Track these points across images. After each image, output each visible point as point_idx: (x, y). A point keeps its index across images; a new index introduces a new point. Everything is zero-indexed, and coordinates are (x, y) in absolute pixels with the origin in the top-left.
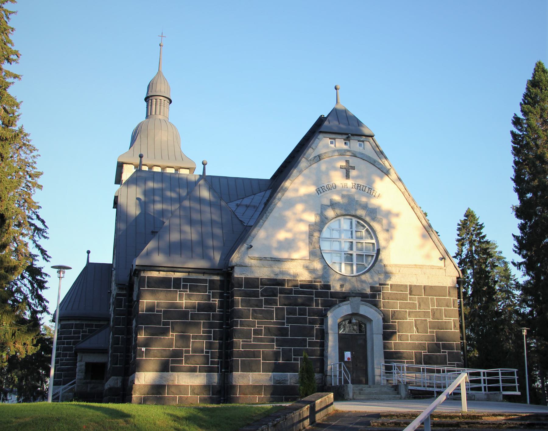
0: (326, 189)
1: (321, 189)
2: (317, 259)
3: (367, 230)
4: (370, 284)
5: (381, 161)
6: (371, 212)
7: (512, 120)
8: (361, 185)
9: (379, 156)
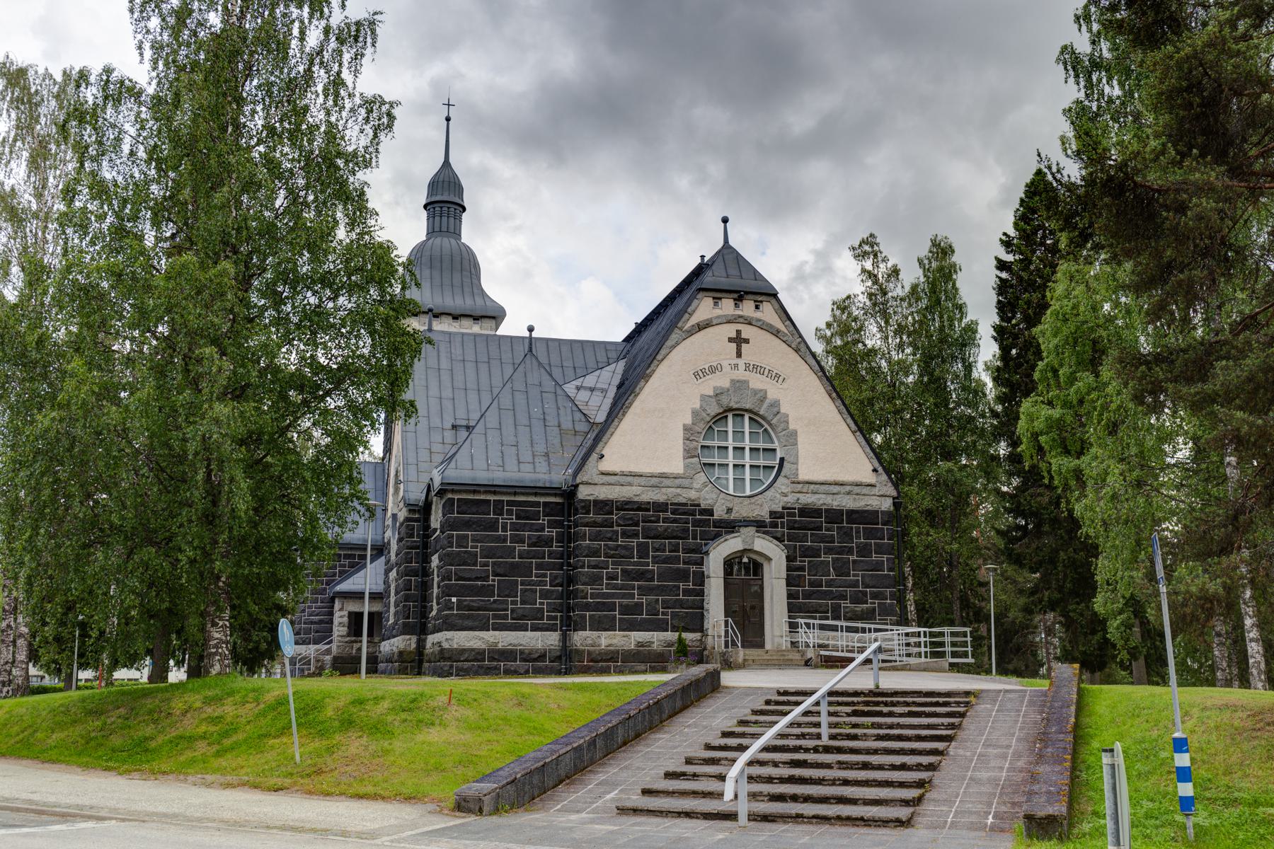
7: (1001, 240)
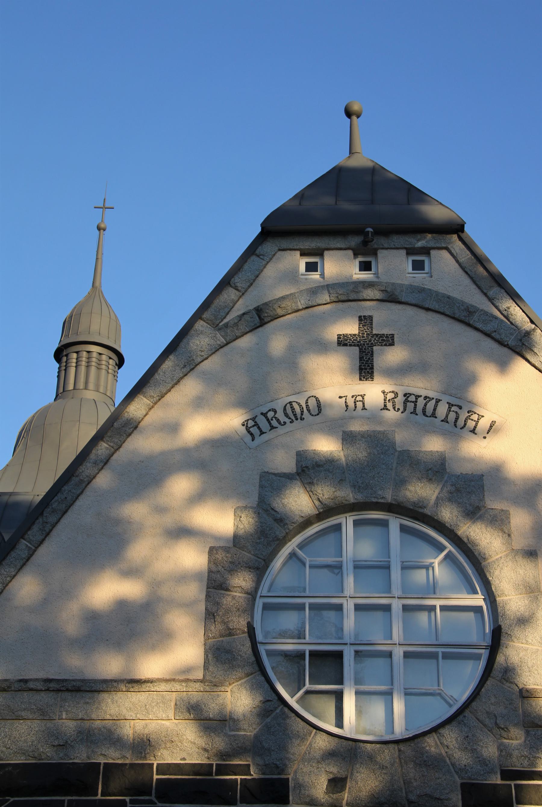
0: (283, 418)
1: (263, 422)
2: (239, 673)
3: (449, 557)
4: (460, 771)
5: (497, 307)
6: (458, 490)
8: (417, 397)
9: (485, 294)
